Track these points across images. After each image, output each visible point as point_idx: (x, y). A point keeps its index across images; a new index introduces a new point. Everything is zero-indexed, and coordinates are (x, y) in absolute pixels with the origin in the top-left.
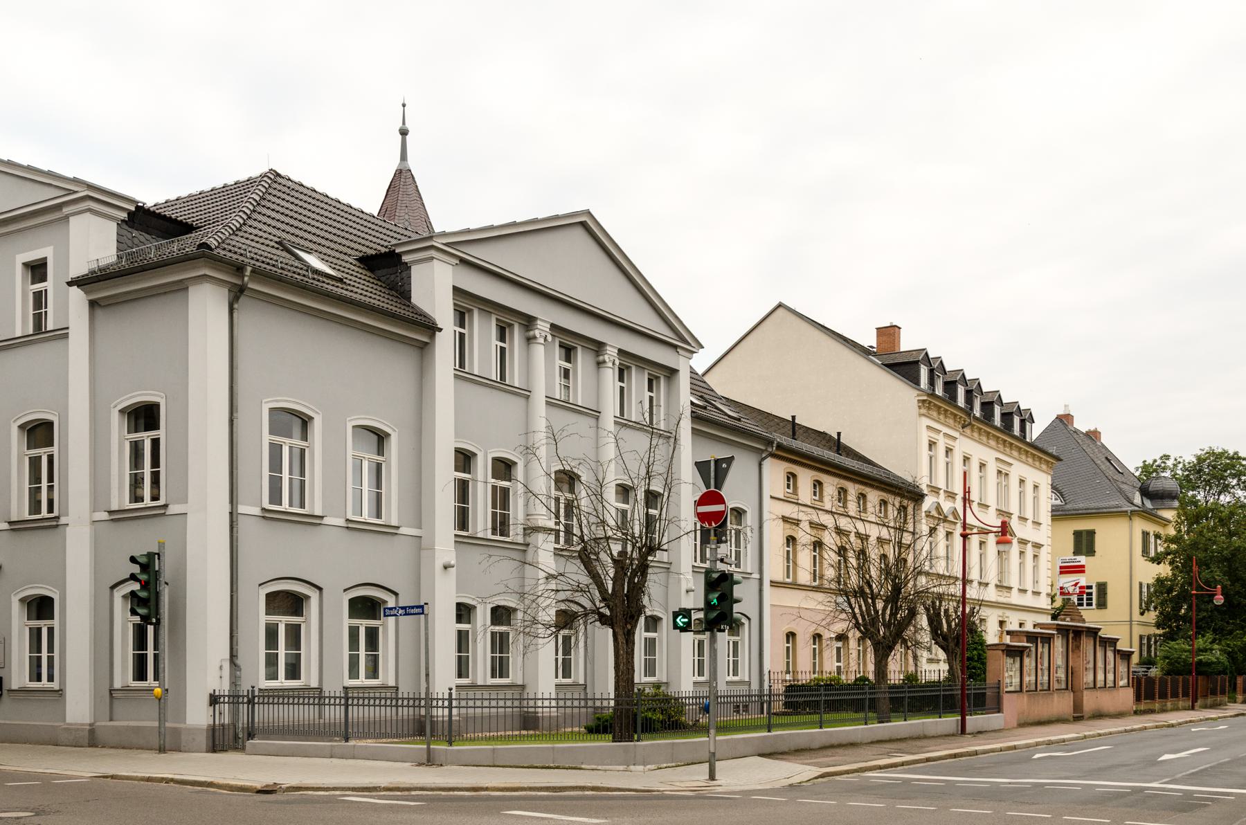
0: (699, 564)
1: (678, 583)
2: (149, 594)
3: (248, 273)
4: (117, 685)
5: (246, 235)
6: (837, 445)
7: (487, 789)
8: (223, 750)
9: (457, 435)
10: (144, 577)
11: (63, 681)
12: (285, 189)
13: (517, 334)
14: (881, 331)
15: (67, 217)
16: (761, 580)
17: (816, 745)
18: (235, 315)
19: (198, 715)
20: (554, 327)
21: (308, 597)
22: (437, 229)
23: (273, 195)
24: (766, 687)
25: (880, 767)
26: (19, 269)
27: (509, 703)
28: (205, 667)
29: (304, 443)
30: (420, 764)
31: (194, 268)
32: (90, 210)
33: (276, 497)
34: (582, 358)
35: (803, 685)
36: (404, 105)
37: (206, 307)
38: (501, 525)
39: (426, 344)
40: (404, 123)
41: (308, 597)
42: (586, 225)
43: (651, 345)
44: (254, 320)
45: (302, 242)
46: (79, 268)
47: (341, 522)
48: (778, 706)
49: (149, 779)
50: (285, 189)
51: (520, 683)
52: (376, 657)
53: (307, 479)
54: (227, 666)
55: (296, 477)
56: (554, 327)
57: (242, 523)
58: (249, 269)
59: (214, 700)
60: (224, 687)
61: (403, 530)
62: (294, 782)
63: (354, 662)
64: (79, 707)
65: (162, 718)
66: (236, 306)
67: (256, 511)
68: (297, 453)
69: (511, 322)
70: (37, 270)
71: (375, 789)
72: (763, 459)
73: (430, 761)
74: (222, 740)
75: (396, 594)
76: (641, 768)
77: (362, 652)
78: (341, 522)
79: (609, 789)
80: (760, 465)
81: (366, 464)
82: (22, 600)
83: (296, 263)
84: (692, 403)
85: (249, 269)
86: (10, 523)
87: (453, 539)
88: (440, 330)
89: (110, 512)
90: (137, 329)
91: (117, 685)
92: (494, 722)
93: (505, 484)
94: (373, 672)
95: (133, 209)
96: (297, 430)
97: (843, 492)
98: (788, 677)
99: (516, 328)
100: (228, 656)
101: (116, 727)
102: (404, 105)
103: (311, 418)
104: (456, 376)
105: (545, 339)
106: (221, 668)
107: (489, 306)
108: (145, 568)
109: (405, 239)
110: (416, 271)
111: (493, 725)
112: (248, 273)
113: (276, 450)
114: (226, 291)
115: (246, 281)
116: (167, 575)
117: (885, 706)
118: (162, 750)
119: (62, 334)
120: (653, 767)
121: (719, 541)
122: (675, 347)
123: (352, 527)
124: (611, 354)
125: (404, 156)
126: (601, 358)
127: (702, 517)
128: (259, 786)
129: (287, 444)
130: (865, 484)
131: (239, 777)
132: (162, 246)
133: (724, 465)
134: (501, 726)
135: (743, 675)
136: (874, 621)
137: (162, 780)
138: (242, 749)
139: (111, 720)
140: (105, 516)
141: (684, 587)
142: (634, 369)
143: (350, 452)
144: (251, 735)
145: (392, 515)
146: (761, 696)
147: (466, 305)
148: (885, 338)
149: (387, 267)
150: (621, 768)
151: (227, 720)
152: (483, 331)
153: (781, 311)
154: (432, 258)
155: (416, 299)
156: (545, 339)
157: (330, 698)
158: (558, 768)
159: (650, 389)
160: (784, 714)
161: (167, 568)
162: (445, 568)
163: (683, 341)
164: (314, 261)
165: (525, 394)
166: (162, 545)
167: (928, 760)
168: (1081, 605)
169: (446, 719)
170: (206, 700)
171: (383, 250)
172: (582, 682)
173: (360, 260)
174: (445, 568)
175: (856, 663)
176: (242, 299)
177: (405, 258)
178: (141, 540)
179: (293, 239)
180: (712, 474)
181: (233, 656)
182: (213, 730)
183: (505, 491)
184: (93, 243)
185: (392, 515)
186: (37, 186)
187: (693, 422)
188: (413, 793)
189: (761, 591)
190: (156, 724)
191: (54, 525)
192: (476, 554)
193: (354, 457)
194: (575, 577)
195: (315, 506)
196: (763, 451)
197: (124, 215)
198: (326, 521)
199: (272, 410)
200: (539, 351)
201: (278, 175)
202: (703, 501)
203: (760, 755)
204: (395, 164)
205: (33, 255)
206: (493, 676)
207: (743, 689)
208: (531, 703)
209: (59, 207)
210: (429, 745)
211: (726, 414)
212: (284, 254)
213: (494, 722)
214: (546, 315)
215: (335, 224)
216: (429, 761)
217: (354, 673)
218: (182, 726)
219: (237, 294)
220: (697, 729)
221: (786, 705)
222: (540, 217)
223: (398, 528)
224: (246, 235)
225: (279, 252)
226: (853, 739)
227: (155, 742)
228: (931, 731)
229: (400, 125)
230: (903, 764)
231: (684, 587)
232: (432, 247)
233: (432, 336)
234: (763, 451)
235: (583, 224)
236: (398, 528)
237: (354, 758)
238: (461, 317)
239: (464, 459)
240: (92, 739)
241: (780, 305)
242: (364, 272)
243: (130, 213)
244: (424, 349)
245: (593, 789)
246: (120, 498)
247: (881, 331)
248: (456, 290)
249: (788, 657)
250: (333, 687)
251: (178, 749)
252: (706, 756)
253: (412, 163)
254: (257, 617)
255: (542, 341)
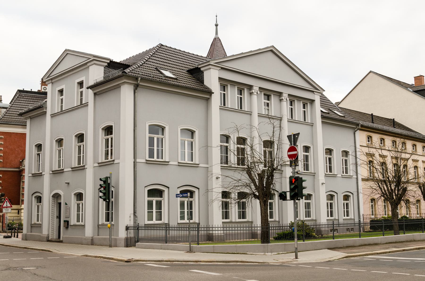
0: (328, 173)
1: (282, 183)
2: (107, 191)
3: (139, 80)
4: (100, 223)
5: (145, 67)
6: (393, 123)
7: (201, 261)
8: (131, 246)
9: (221, 130)
10: (104, 185)
11: (85, 223)
12: (164, 50)
13: (246, 92)
14: (416, 78)
15: (89, 67)
16: (357, 178)
17: (358, 244)
18: (136, 94)
19: (122, 234)
20: (260, 88)
21: (164, 191)
22: (228, 55)
23: (161, 53)
24: (362, 220)
25: (378, 254)
26: (76, 84)
27: (247, 229)
28: (125, 217)
29: (163, 136)
30: (188, 252)
31: (121, 80)
32: (95, 64)
33: (151, 155)
34: (273, 98)
35: (414, 220)
36: (216, 16)
37: (126, 92)
38: (241, 161)
39: (209, 98)
40: (216, 22)
41: (164, 191)
42: (273, 51)
43: (305, 93)
44: (143, 95)
45: (163, 66)
46: (91, 83)
47: (177, 163)
48: (368, 228)
49: (96, 257)
50: (164, 50)
51: (250, 220)
52: (161, 212)
53: (163, 149)
54: (132, 216)
55: (160, 148)
56: (260, 88)
57: (138, 165)
58: (140, 78)
59: (127, 228)
60: (131, 224)
61: (200, 165)
62: (137, 258)
63: (182, 213)
64: (89, 232)
65: (110, 235)
66: (136, 91)
67: (144, 161)
68: (160, 140)
69: (242, 88)
70: (81, 84)
71: (162, 261)
72: (356, 131)
73: (191, 251)
74: (130, 243)
75: (198, 189)
76: (270, 254)
77: (154, 210)
78: (177, 163)
79: (247, 262)
80: (354, 134)
81: (186, 142)
82: (75, 194)
83: (161, 75)
84: (322, 111)
85: (140, 78)
86: (72, 168)
87: (220, 167)
88: (213, 93)
89: (99, 163)
90: (107, 100)
91: (100, 223)
92: (239, 236)
93: (242, 146)
94: (159, 218)
95: (109, 62)
96: (160, 132)
97: (394, 142)
98: (418, 216)
99: (246, 90)
100: (133, 213)
101: (99, 238)
102: (216, 16)
103: (165, 127)
104: (220, 109)
105: (257, 93)
106: (130, 217)
107: (233, 83)
108: (105, 182)
109: (201, 63)
110: (205, 73)
111: (239, 237)
112: (139, 80)
113: (151, 140)
114: (133, 86)
115: (139, 83)
116: (113, 183)
117: (396, 228)
118: (110, 246)
119: (86, 105)
120: (275, 253)
121: (296, 166)
122: (313, 92)
123: (180, 165)
124: (285, 96)
125: (217, 33)
126: (281, 98)
127: (290, 156)
128: (126, 259)
129: (156, 137)
130: (405, 139)
131: (124, 256)
132: (118, 72)
133: (297, 136)
134: (242, 237)
135: (351, 216)
136: (391, 194)
137: (99, 257)
138: (135, 246)
139: (98, 235)
140: (97, 165)
141: (321, 182)
142: (296, 101)
143: (180, 138)
144: (138, 241)
145: (196, 160)
146: (360, 223)
147: (224, 83)
148: (418, 81)
149: (196, 73)
150: (262, 254)
151: (132, 235)
152: (232, 94)
153: (371, 74)
154: (210, 68)
155: (206, 83)
156: (257, 93)
157: (171, 227)
158: (238, 253)
159: (304, 108)
160: (370, 232)
161: (113, 182)
162: (217, 178)
163: (315, 88)
164: (168, 74)
165: (250, 113)
166: (111, 174)
167: (404, 250)
168: (242, 195)
169: (197, 234)
170: (124, 228)
171: (192, 68)
172: (277, 220)
173: (188, 71)
174: (217, 178)
175: (382, 211)
176: (138, 89)
177: (202, 69)
178: (104, 173)
179: (160, 66)
180: (293, 140)
181: (135, 212)
182: (127, 239)
183: (243, 149)
184: (96, 74)
185: (196, 160)
186: (81, 58)
187: (322, 119)
188: (238, 263)
189: (357, 183)
190: (108, 237)
191: (83, 168)
192: (230, 173)
193: (181, 140)
194: (244, 181)
195: (166, 158)
196: (355, 128)
197: (106, 64)
198: (170, 163)
199: (150, 126)
200: (255, 97)
201: (162, 45)
202: (289, 150)
203: (328, 249)
204: (213, 36)
205: (79, 80)
206: (306, 217)
207: (352, 222)
208: (256, 228)
209: (86, 64)
210: (190, 244)
211: (338, 115)
212: (157, 72)
213: (239, 236)
214: (257, 84)
215: (189, 59)
216: (190, 250)
217: (182, 218)
218: (118, 238)
219: (136, 87)
220: (315, 238)
221: (371, 228)
222: (253, 50)
223: (199, 164)
224: (145, 67)
225: (156, 72)
226: (376, 242)
227: (108, 243)
228: (418, 238)
229: (215, 23)
230: (390, 252)
231: (321, 182)
232: (210, 64)
233: (211, 95)
234: (355, 128)
235: (271, 51)
236: (199, 164)
237: (168, 249)
238: (224, 88)
239: (226, 138)
240: (92, 242)
241: (370, 72)
242: (188, 75)
243: (108, 63)
244: (208, 100)
245: (241, 262)
246: (102, 159)
247: (416, 78)
248: (219, 78)
249: (372, 209)
250: (173, 223)
251: (116, 246)
252: (294, 250)
253: (220, 36)
254: (144, 198)
255: (256, 94)
